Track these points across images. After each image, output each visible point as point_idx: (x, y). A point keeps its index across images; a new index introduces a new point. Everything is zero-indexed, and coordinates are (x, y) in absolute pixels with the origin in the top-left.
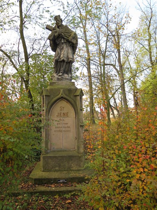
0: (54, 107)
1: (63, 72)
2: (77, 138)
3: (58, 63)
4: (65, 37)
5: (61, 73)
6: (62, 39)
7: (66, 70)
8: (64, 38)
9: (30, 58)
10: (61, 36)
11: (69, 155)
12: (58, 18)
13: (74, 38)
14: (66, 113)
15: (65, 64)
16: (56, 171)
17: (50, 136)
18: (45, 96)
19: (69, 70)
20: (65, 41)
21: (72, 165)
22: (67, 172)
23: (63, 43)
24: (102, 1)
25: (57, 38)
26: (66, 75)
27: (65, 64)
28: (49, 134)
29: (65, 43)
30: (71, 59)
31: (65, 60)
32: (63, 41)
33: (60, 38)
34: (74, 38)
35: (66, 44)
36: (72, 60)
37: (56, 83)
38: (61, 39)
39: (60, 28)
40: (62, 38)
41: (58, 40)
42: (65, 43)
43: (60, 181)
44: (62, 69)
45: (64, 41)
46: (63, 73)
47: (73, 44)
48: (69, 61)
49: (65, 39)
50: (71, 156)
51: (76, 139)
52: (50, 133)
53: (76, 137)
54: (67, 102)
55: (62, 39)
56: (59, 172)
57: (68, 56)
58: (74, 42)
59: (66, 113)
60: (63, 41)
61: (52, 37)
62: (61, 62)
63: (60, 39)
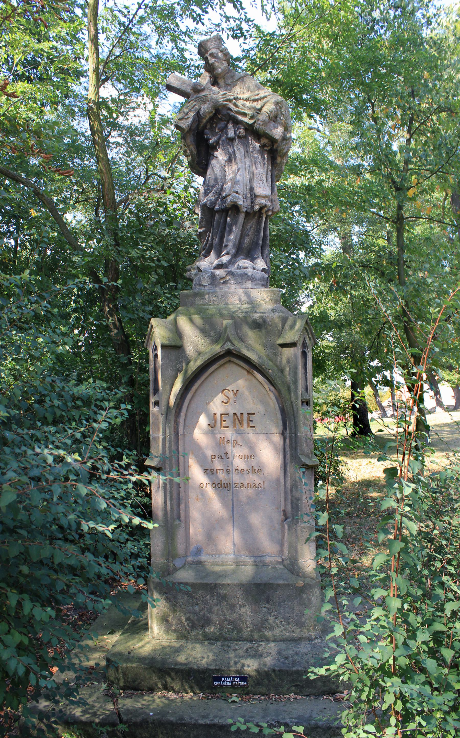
0: (196, 390)
1: (233, 251)
2: (289, 514)
3: (213, 216)
4: (240, 117)
5: (227, 254)
6: (230, 126)
7: (247, 241)
8: (237, 122)
9: (34, 561)
10: (225, 112)
11: (259, 582)
12: (199, 163)
13: (276, 117)
14: (245, 416)
15: (241, 218)
16: (209, 639)
17: (182, 506)
18: (163, 346)
19: (257, 244)
20: (242, 131)
21: (271, 619)
22: (249, 645)
23: (231, 140)
24: (457, 625)
25: (207, 122)
26: (244, 263)
27: (241, 218)
28: (179, 494)
29: (240, 137)
30: (263, 201)
31: (240, 203)
32: (231, 133)
33: (221, 120)
34: (276, 117)
35: (242, 144)
36: (269, 204)
37: (207, 297)
38: (226, 126)
39: (221, 82)
40: (228, 122)
41: (212, 129)
42: (240, 137)
43: (220, 680)
44: (232, 238)
45: (235, 132)
46: (235, 256)
47: (273, 141)
48: (257, 207)
49: (241, 122)
50: (265, 584)
51: (286, 519)
52: (182, 494)
53: (284, 511)
54: (248, 372)
55: (230, 126)
56: (219, 643)
57: (252, 189)
58: (278, 132)
59: (245, 416)
60: (231, 133)
61: (190, 121)
62: (225, 211)
63: (222, 124)
